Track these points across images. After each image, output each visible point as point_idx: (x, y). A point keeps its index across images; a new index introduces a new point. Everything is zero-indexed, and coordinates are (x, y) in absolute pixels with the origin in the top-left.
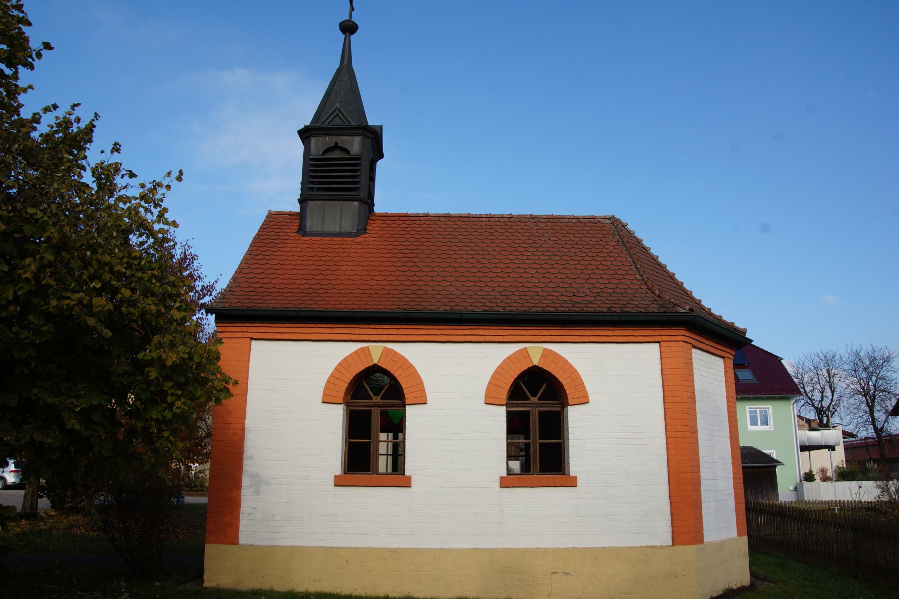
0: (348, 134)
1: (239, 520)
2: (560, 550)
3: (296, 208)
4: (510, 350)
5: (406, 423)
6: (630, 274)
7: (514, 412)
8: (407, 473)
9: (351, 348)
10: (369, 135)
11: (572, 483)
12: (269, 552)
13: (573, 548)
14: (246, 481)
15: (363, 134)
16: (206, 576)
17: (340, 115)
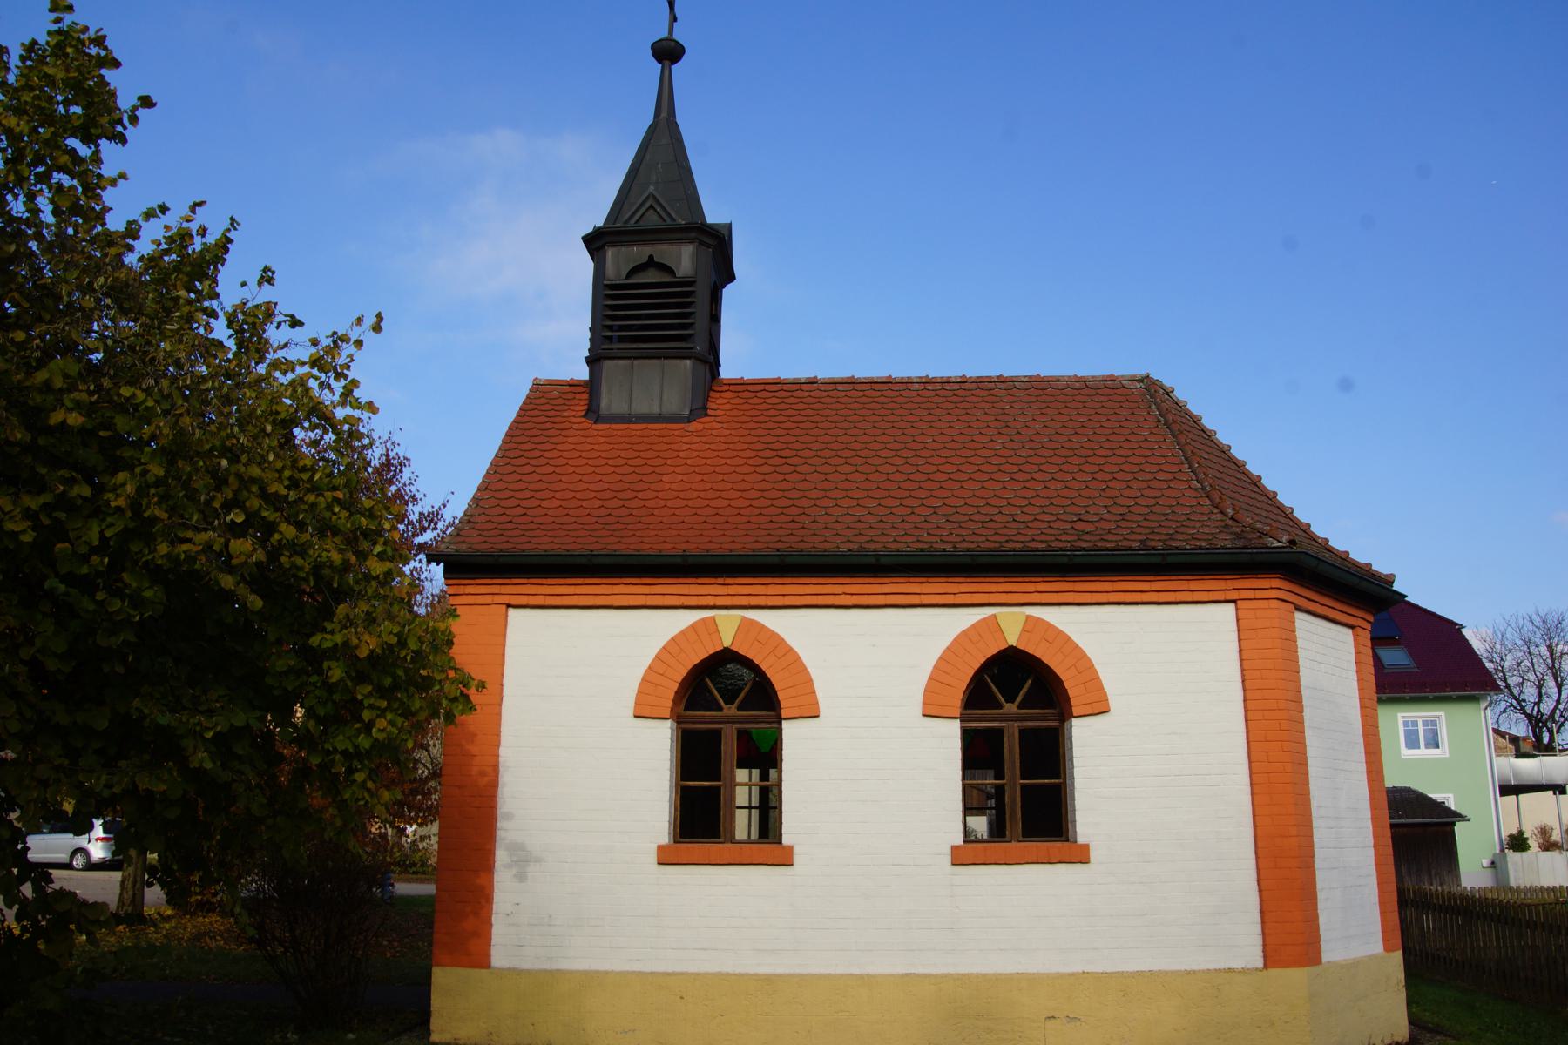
2: (1060, 976)
7: (976, 731)
11: (1081, 856)
12: (546, 981)
13: (1084, 972)
16: (435, 1023)
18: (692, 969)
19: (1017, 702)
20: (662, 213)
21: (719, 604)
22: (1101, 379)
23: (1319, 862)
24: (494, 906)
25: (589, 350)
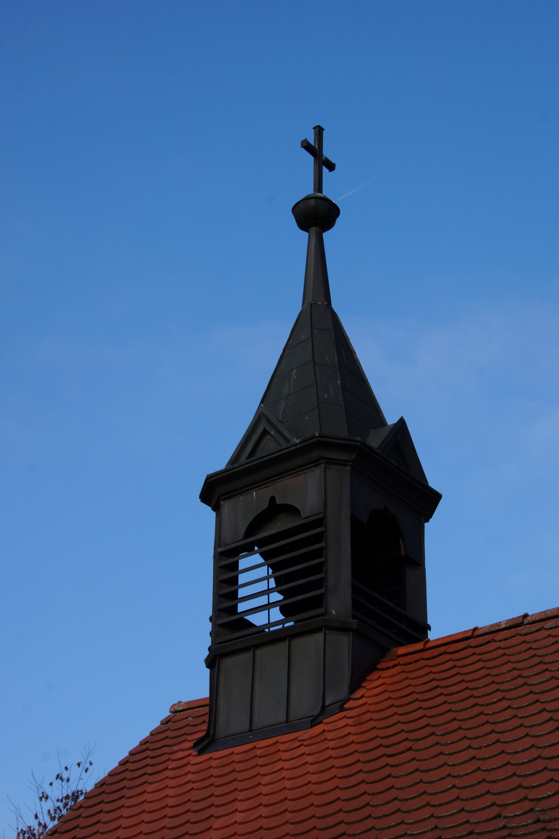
0: (294, 471)
10: (344, 456)
15: (324, 458)
17: (269, 429)
25: (209, 649)
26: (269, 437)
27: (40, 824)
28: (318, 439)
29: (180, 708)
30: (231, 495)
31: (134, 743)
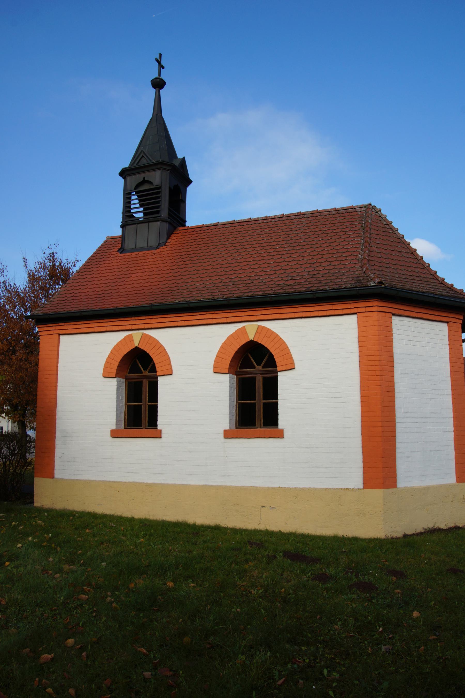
0: (152, 170)
1: (54, 461)
2: (268, 488)
3: (119, 232)
4: (232, 329)
5: (158, 390)
6: (353, 255)
7: (243, 379)
8: (159, 427)
9: (121, 335)
11: (280, 435)
12: (72, 483)
13: (280, 487)
14: (58, 435)
15: (162, 168)
16: (35, 499)
17: (144, 156)
18: (124, 480)
19: (262, 365)
20: (147, 159)
21: (133, 328)
22: (346, 208)
23: (398, 440)
24: (56, 454)
25: (122, 222)
26: (144, 158)
27: (43, 261)
28: (161, 162)
29: (109, 238)
30: (129, 175)
31: (97, 248)
